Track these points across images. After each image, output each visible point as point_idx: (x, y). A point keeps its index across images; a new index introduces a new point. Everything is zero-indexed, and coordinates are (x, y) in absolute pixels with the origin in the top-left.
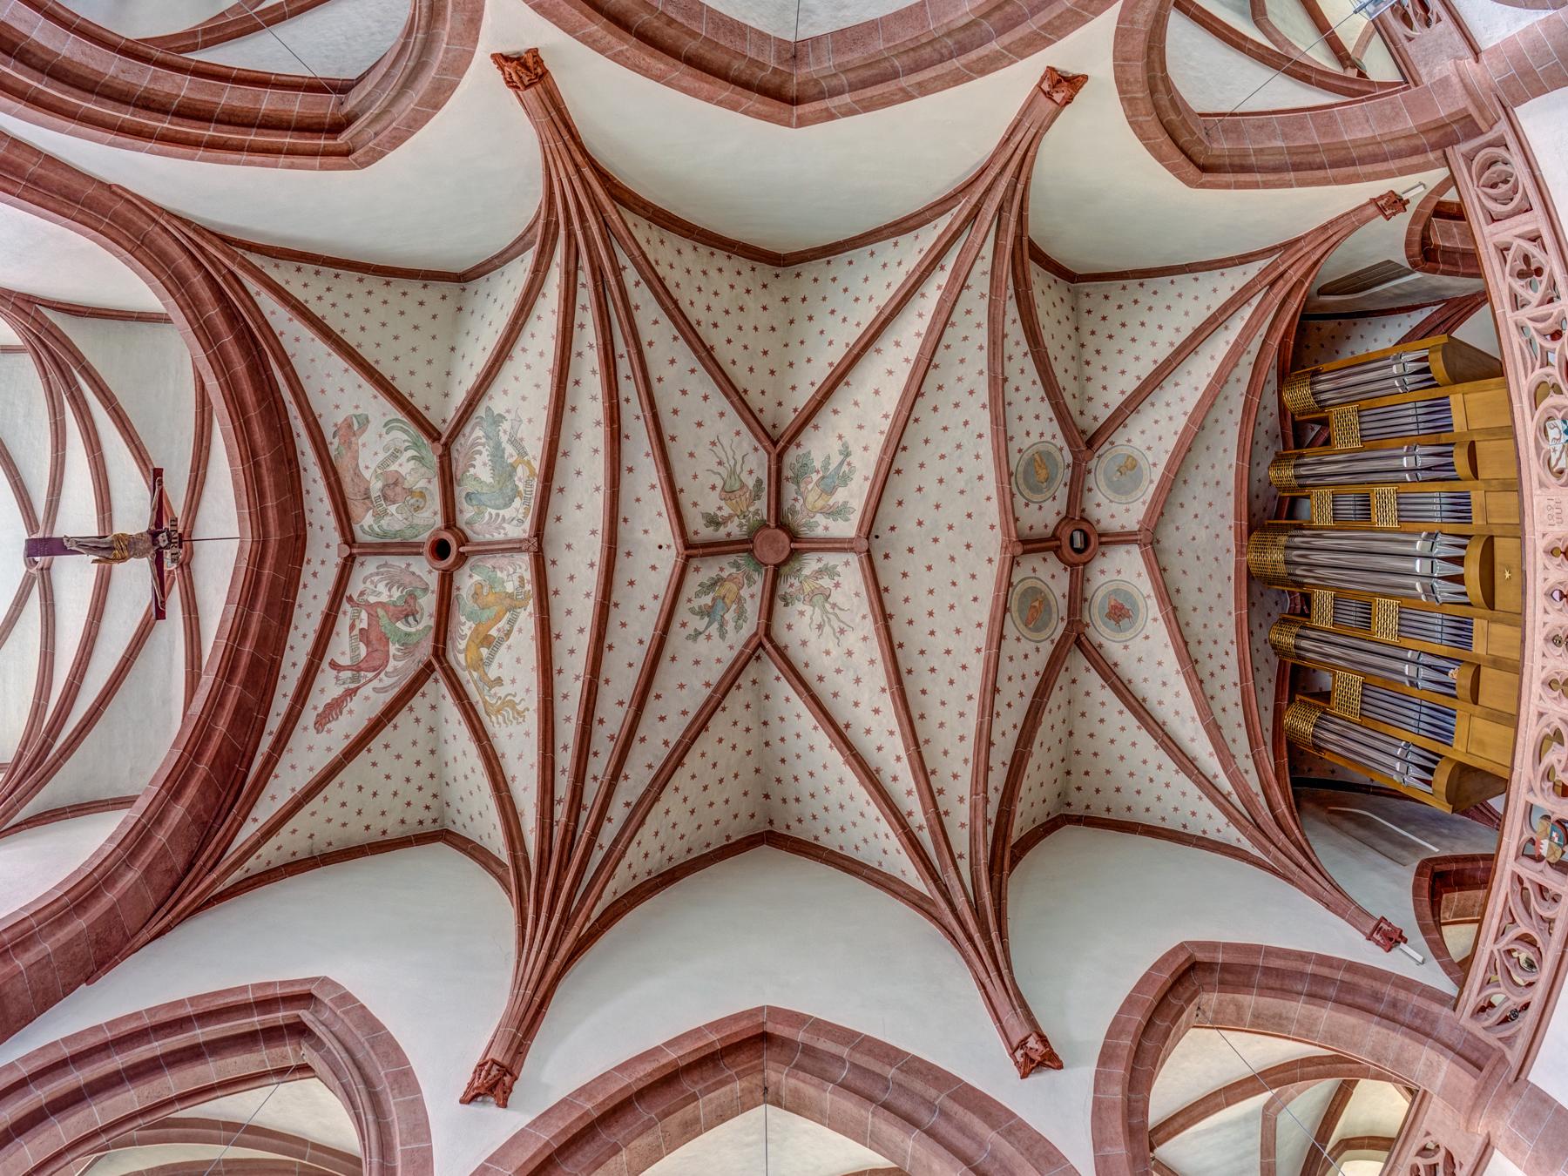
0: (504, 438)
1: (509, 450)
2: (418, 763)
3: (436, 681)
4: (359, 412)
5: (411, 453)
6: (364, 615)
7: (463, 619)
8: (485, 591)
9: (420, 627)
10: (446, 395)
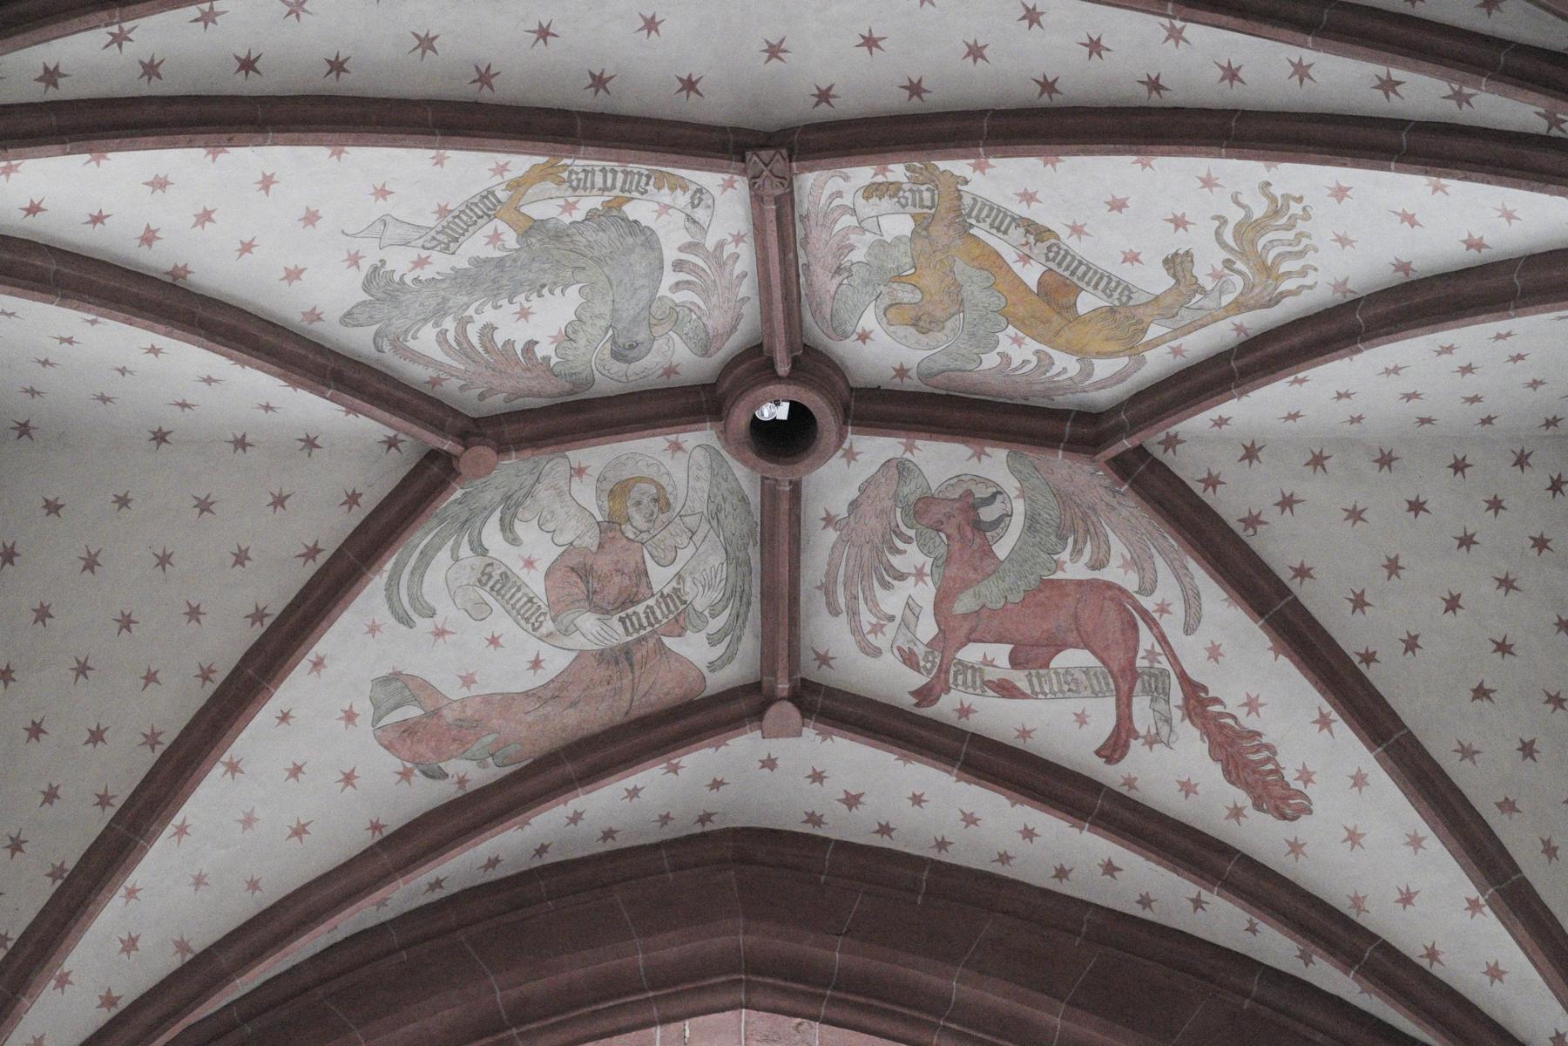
0: (441, 264)
1: (476, 245)
2: (1416, 507)
3: (1171, 442)
4: (364, 708)
5: (492, 535)
6: (972, 653)
7: (990, 361)
8: (907, 295)
9: (1010, 485)
10: (310, 443)
